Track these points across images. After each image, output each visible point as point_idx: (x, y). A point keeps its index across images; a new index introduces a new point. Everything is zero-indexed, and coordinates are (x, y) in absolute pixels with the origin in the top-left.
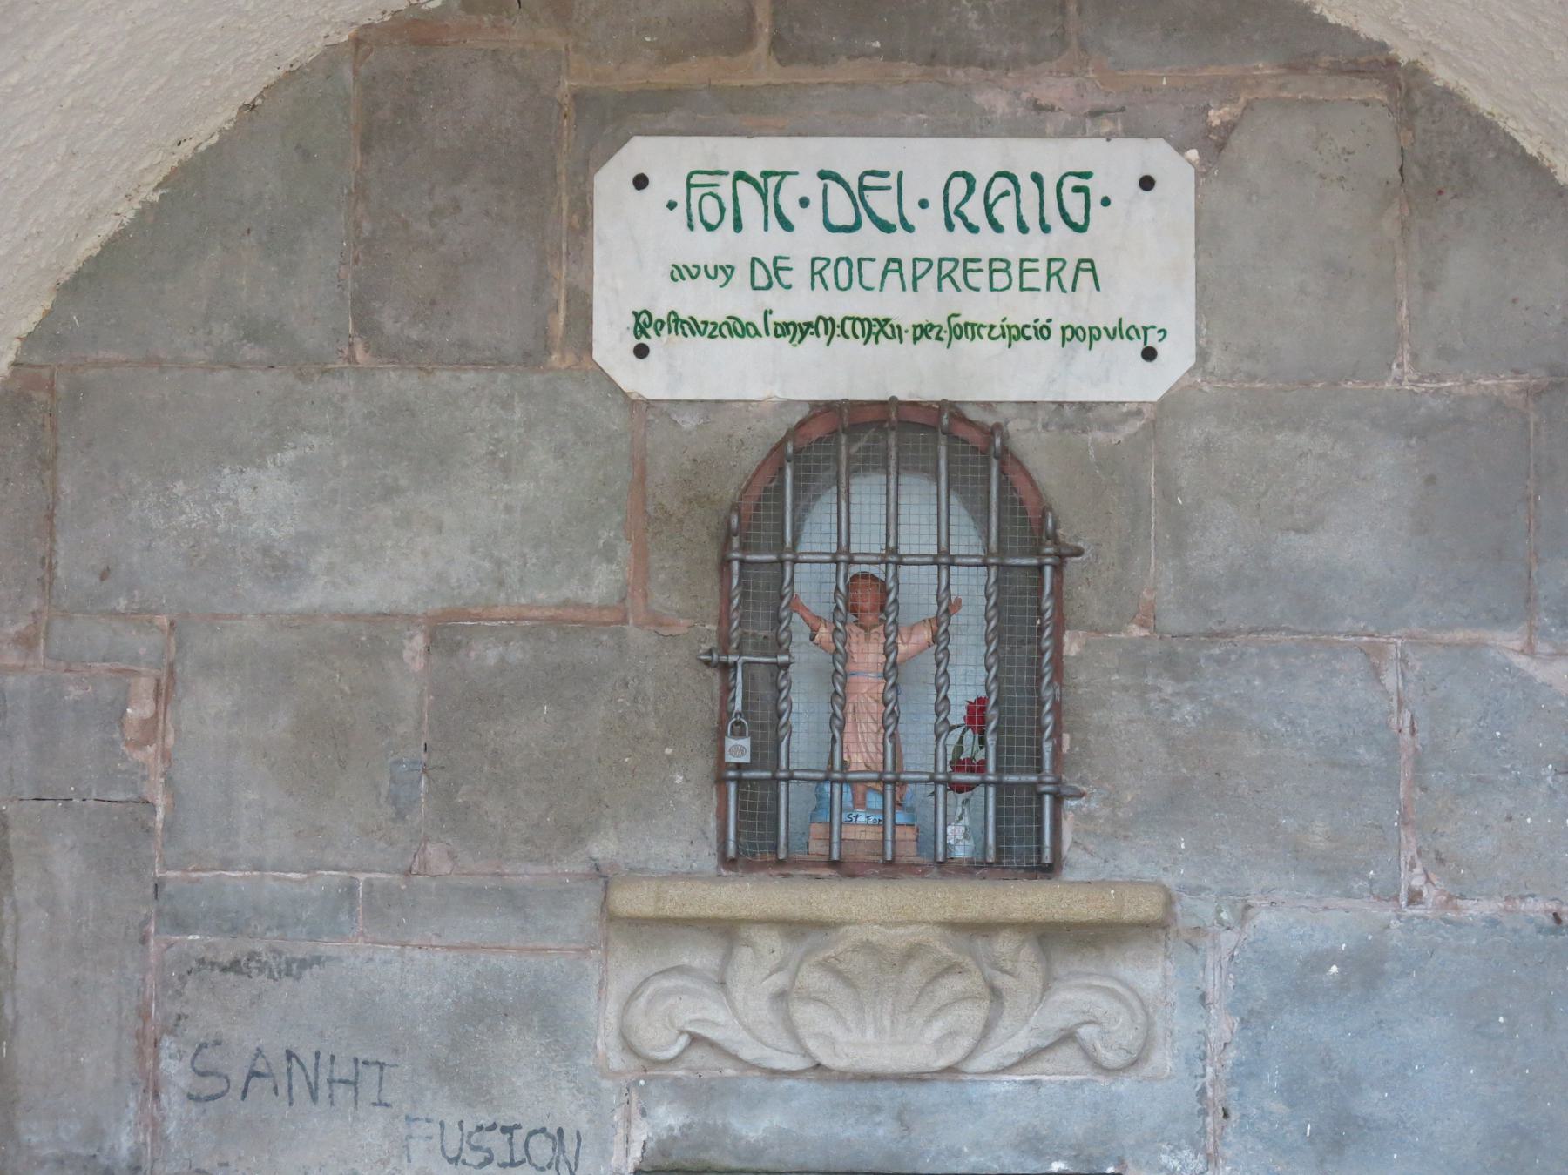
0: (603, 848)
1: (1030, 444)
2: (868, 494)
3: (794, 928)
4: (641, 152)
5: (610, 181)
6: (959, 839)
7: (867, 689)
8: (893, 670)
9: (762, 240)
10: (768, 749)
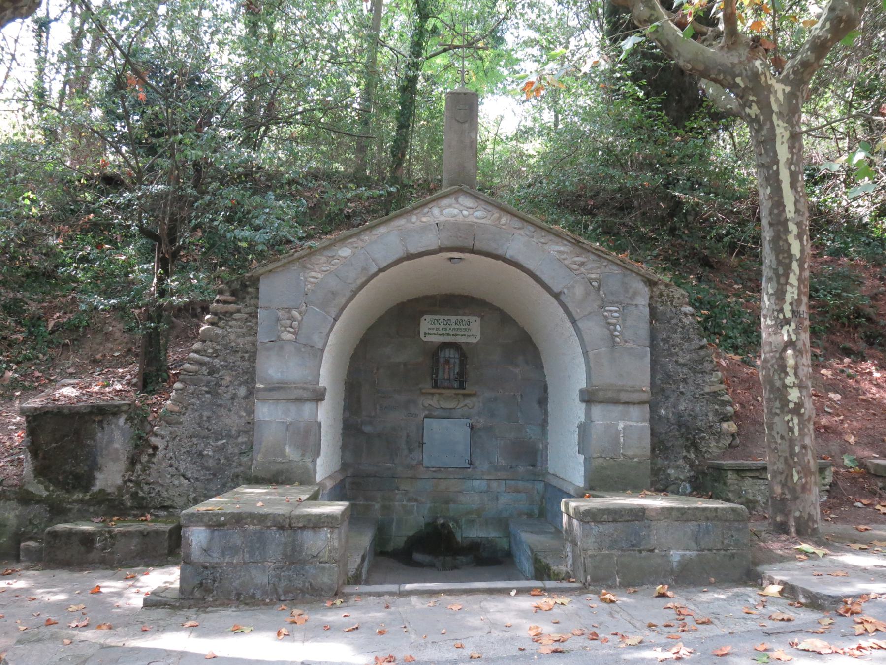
0: (421, 386)
1: (464, 347)
2: (447, 351)
3: (439, 394)
4: (425, 317)
5: (422, 319)
6: (455, 386)
7: (447, 370)
8: (449, 369)
9: (437, 326)
10: (437, 376)
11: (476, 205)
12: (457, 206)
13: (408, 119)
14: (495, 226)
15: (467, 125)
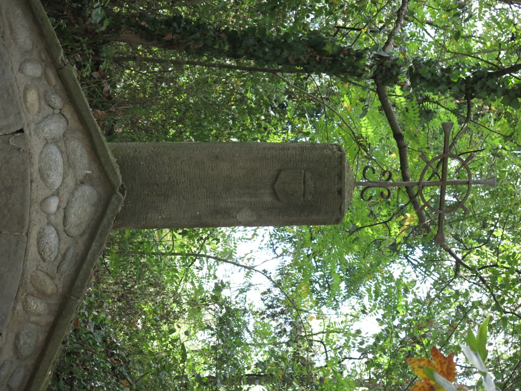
11: (75, 232)
12: (70, 182)
13: (251, 56)
14: (22, 284)
15: (268, 199)
